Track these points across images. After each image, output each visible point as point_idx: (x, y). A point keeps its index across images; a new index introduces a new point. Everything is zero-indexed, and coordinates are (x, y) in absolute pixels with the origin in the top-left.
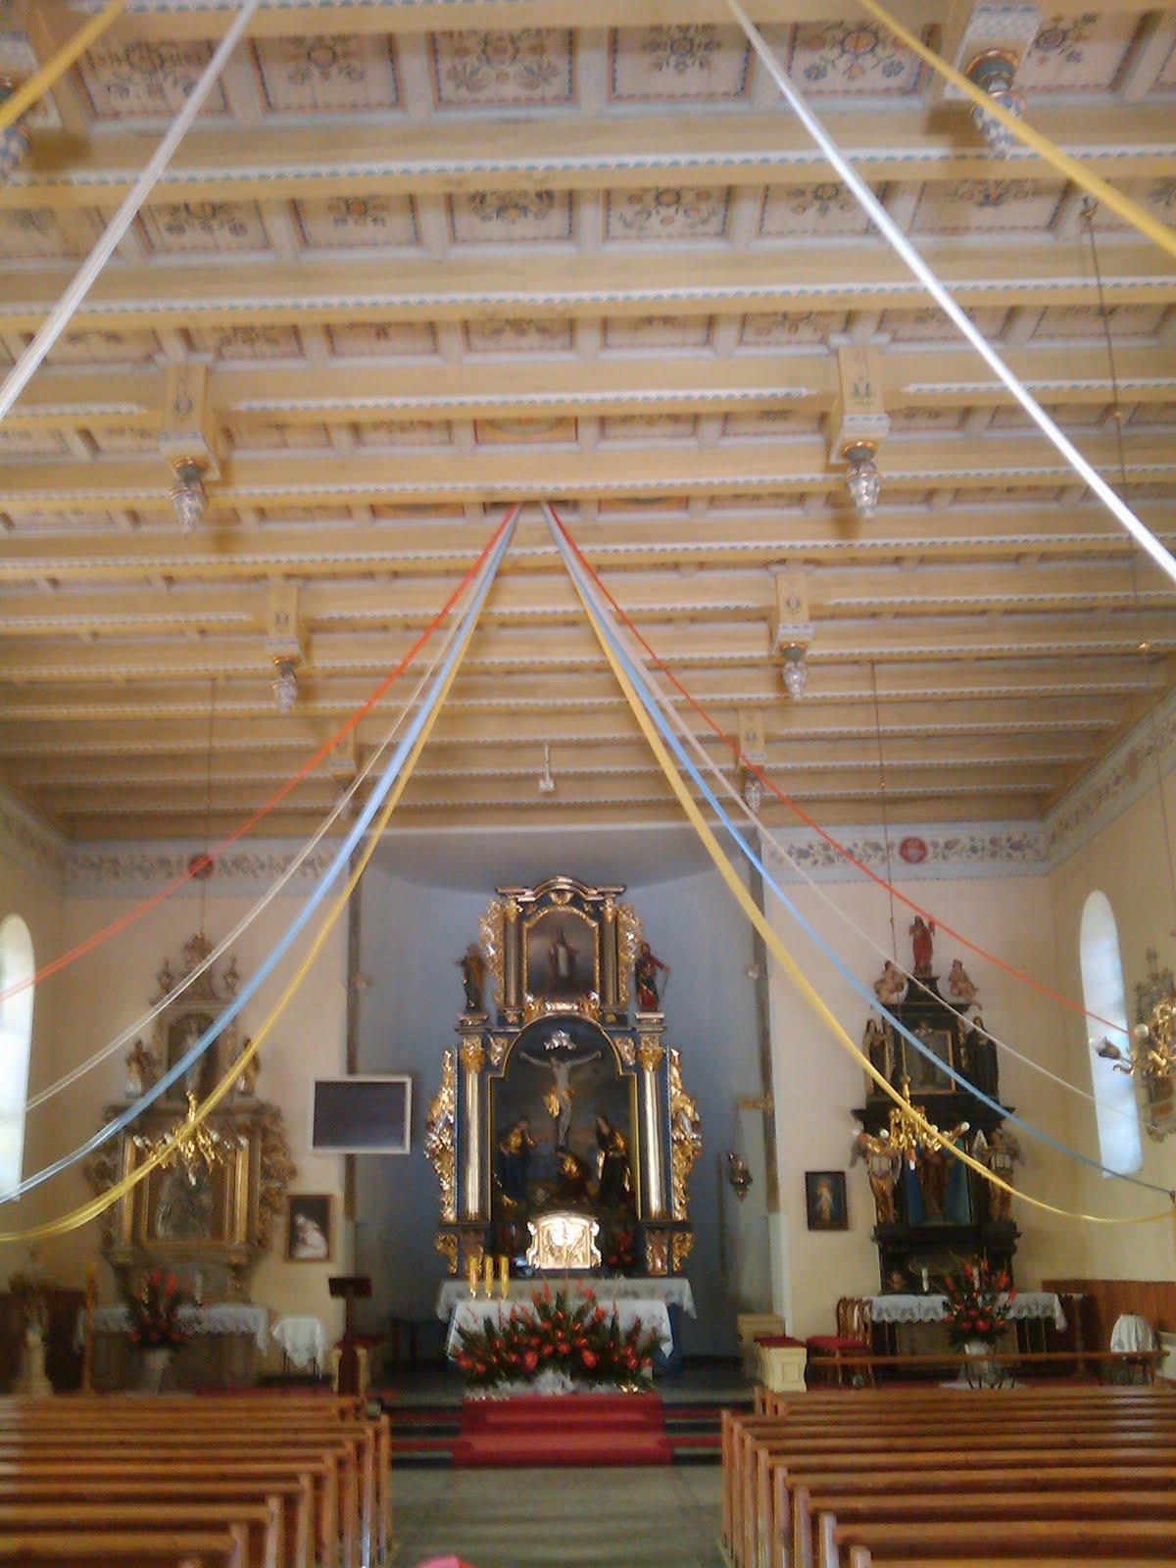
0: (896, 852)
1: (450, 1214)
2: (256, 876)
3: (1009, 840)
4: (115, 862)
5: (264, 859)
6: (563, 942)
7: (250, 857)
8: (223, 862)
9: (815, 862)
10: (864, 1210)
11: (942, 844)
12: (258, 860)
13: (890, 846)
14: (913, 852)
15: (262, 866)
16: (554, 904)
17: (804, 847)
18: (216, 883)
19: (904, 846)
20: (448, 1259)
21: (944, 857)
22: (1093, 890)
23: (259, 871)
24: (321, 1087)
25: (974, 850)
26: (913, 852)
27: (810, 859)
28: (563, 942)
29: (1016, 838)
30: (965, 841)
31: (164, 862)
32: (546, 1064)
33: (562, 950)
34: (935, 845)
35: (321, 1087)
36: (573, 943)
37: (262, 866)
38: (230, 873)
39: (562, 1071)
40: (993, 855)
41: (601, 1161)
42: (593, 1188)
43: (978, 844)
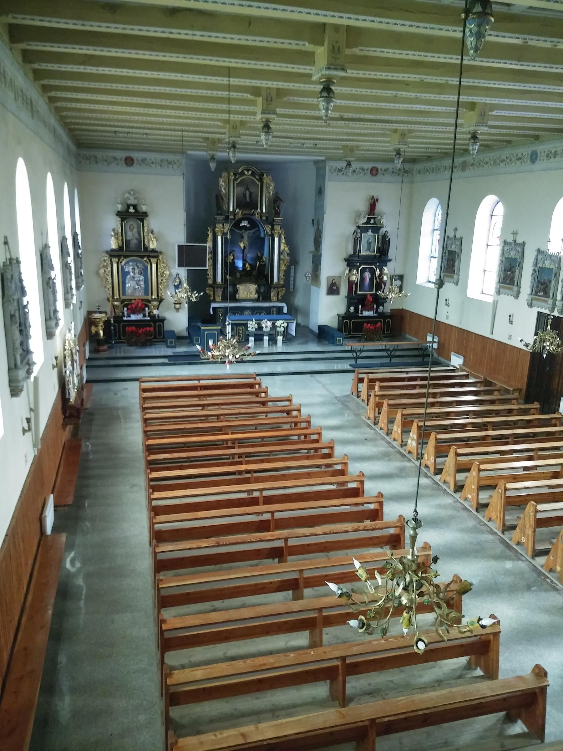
0: (369, 171)
1: (210, 282)
2: (150, 166)
3: (404, 169)
4: (96, 157)
5: (153, 160)
6: (248, 189)
7: (148, 159)
8: (138, 160)
9: (343, 174)
10: (344, 291)
11: (383, 170)
12: (150, 160)
13: (367, 169)
14: (374, 172)
15: (153, 163)
16: (246, 175)
17: (340, 168)
18: (135, 168)
19: (372, 170)
20: (210, 296)
21: (384, 175)
22: (438, 199)
23: (151, 165)
24: (179, 246)
25: (393, 172)
26: (374, 172)
27: (342, 173)
28: (248, 189)
29: (407, 169)
30: (391, 169)
31: (115, 159)
32: (240, 232)
33: (247, 192)
34: (381, 170)
35: (179, 246)
36: (251, 190)
37: (153, 163)
38: (140, 165)
39: (246, 235)
40: (399, 175)
41: (258, 265)
42: (255, 273)
43: (395, 170)
